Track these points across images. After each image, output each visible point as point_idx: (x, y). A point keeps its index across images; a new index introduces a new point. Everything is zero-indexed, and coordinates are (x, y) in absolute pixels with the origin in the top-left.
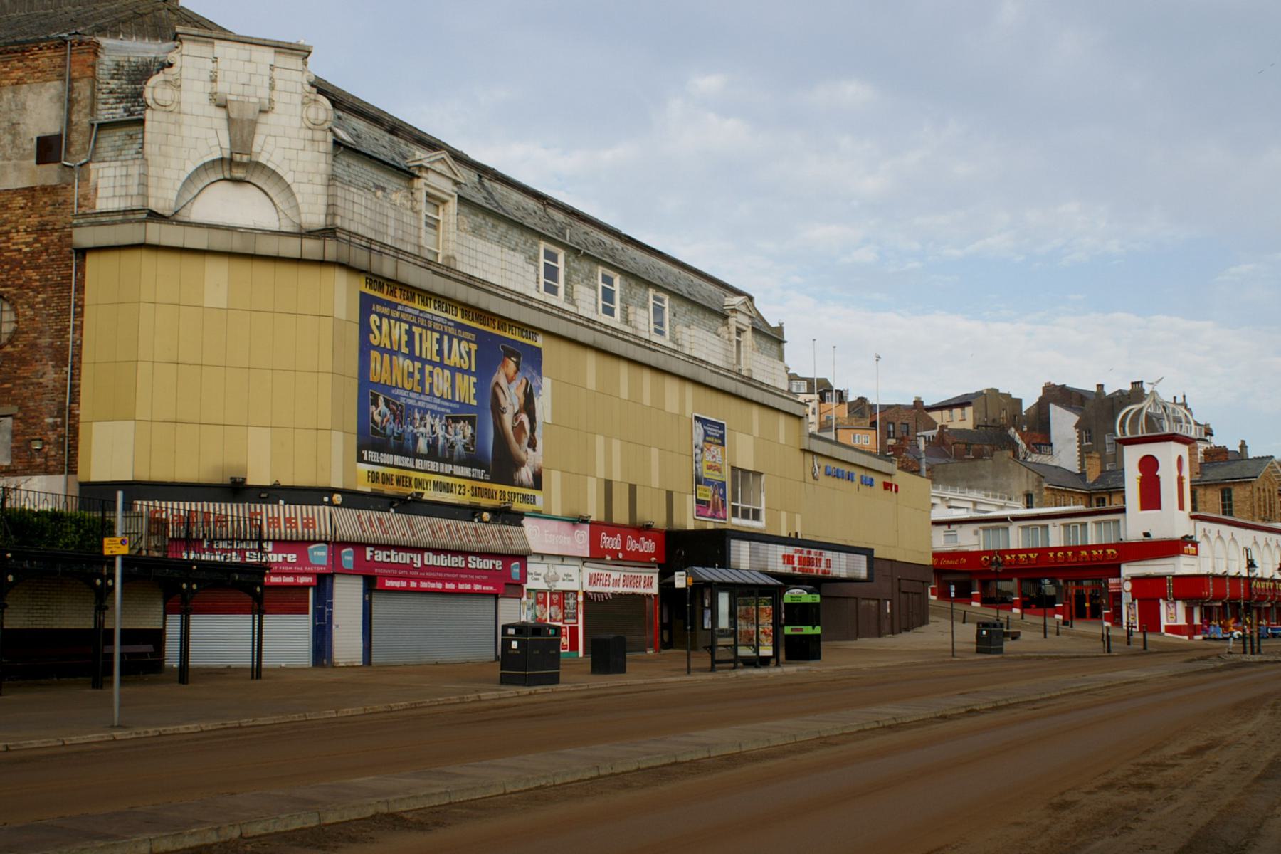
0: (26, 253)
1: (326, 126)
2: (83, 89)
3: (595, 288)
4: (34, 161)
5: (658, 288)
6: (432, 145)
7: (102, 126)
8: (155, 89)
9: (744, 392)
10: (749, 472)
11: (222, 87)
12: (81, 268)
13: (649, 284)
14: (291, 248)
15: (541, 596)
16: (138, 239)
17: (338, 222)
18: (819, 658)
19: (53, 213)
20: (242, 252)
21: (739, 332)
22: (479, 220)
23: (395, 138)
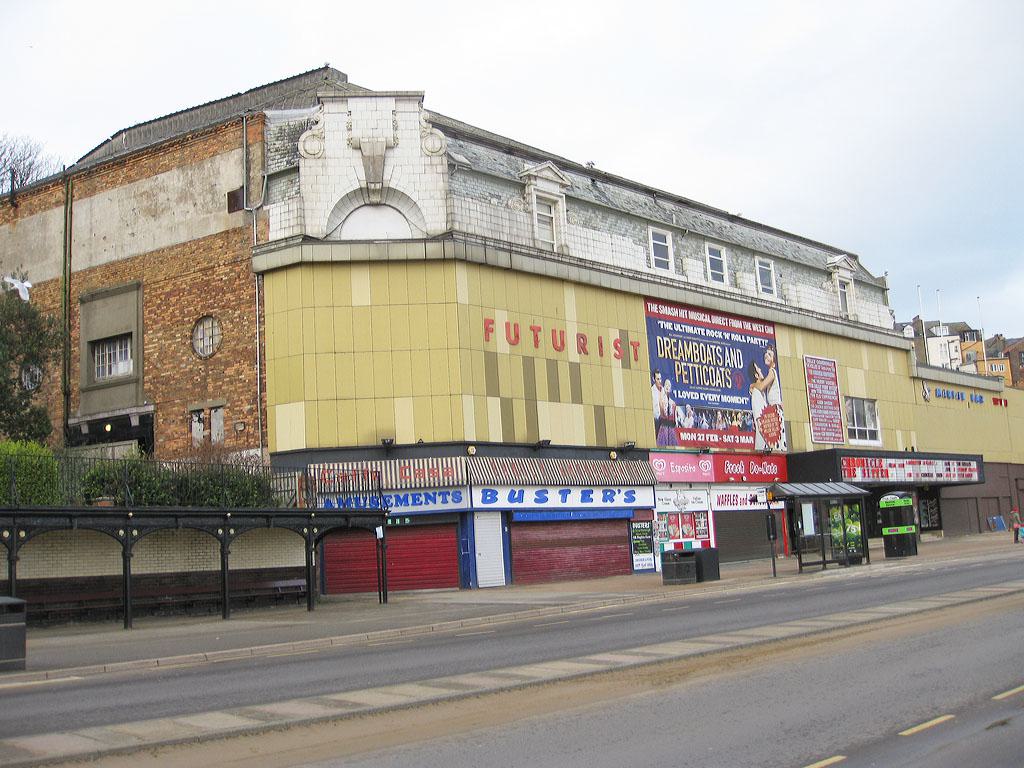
0: (225, 281)
1: (441, 152)
2: (256, 151)
3: (704, 261)
4: (227, 211)
5: (762, 254)
6: (536, 156)
7: (271, 177)
8: (306, 143)
9: (848, 333)
10: (863, 400)
11: (356, 134)
12: (261, 288)
13: (754, 252)
14: (417, 252)
15: (673, 518)
16: (297, 259)
17: (457, 227)
18: (718, 577)
19: (241, 248)
20: (380, 261)
21: (843, 285)
22: (590, 214)
23: (513, 157)
